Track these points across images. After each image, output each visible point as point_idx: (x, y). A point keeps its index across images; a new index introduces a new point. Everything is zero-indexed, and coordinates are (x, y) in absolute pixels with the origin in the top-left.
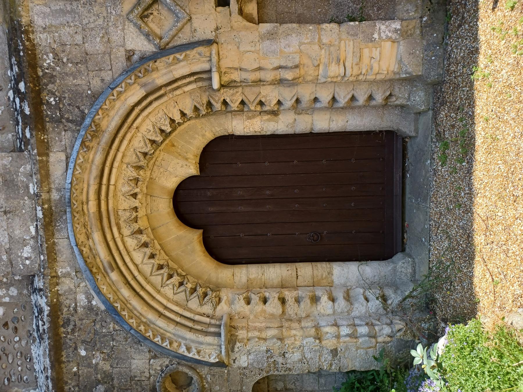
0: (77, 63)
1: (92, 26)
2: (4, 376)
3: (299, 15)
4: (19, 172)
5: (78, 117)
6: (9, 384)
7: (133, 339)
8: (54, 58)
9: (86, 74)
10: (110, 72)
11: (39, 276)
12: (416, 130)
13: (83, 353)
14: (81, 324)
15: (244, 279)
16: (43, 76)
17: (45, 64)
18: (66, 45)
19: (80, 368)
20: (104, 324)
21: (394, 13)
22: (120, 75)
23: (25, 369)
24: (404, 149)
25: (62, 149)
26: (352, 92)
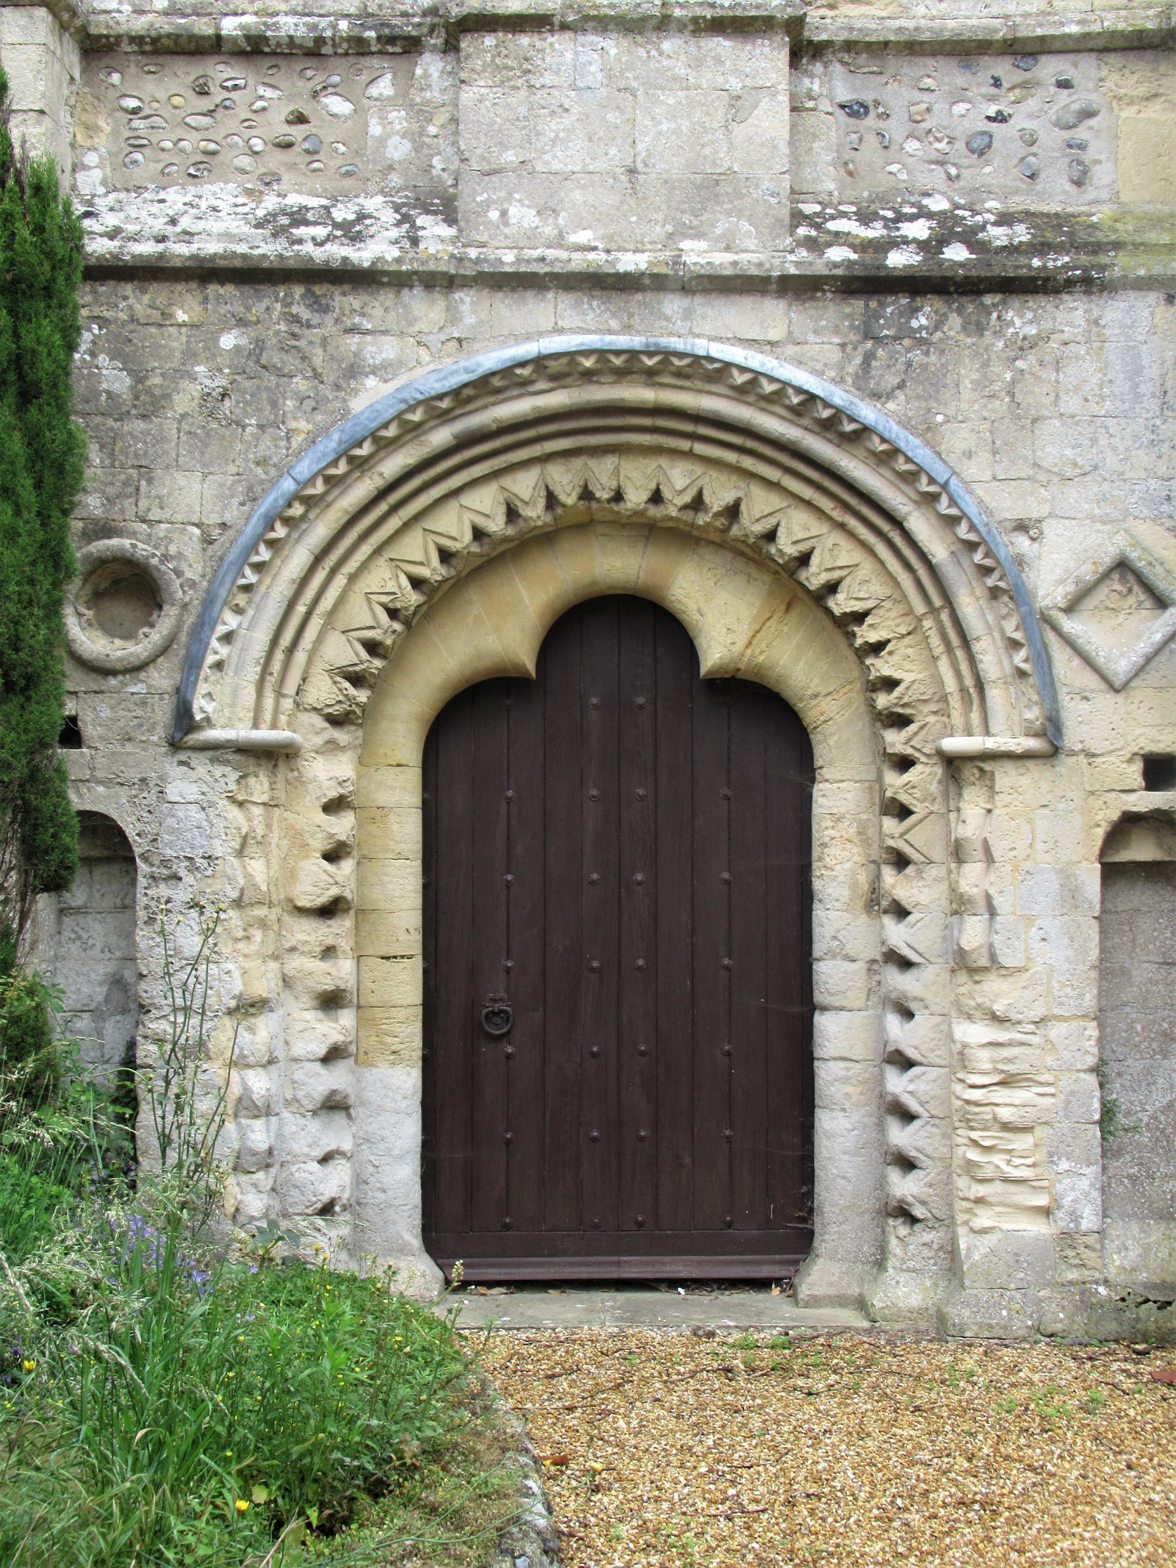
0: (1012, 395)
1: (1103, 442)
2: (147, 99)
3: (1124, 972)
4: (739, 219)
5: (878, 384)
6: (126, 110)
7: (262, 482)
8: (1025, 338)
9: (986, 414)
10: (988, 476)
11: (454, 240)
12: (815, 1302)
13: (228, 341)
14: (311, 343)
15: (384, 797)
16: (982, 304)
17: (1011, 314)
18: (1057, 371)
19: (184, 330)
20: (309, 404)
21: (1123, 1215)
22: (981, 502)
23: (166, 158)
24: (761, 1284)
25: (796, 334)
26: (926, 1114)
